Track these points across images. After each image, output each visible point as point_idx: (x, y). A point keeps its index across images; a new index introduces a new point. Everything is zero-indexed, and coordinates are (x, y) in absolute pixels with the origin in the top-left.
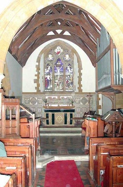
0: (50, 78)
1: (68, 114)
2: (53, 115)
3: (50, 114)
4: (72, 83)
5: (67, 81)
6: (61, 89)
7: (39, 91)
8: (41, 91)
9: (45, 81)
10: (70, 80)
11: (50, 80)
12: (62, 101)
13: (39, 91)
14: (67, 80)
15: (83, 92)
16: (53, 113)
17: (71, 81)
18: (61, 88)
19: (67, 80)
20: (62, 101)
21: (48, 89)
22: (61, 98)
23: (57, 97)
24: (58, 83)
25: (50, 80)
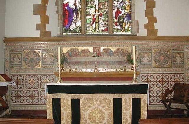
0: (75, 4)
1: (127, 99)
2: (76, 105)
3: (66, 99)
4: (129, 16)
5: (118, 12)
6: (102, 31)
7: (45, 35)
8: (53, 35)
9: (64, 11)
10: (125, 9)
11: (76, 10)
12: (105, 59)
13: (45, 35)
14: (116, 9)
15: (158, 35)
16: (76, 96)
17: (126, 11)
18: (103, 28)
19: (118, 9)
20: (105, 59)
21: (71, 31)
22: (102, 51)
23: (91, 50)
24: (94, 15)
25: (76, 10)
